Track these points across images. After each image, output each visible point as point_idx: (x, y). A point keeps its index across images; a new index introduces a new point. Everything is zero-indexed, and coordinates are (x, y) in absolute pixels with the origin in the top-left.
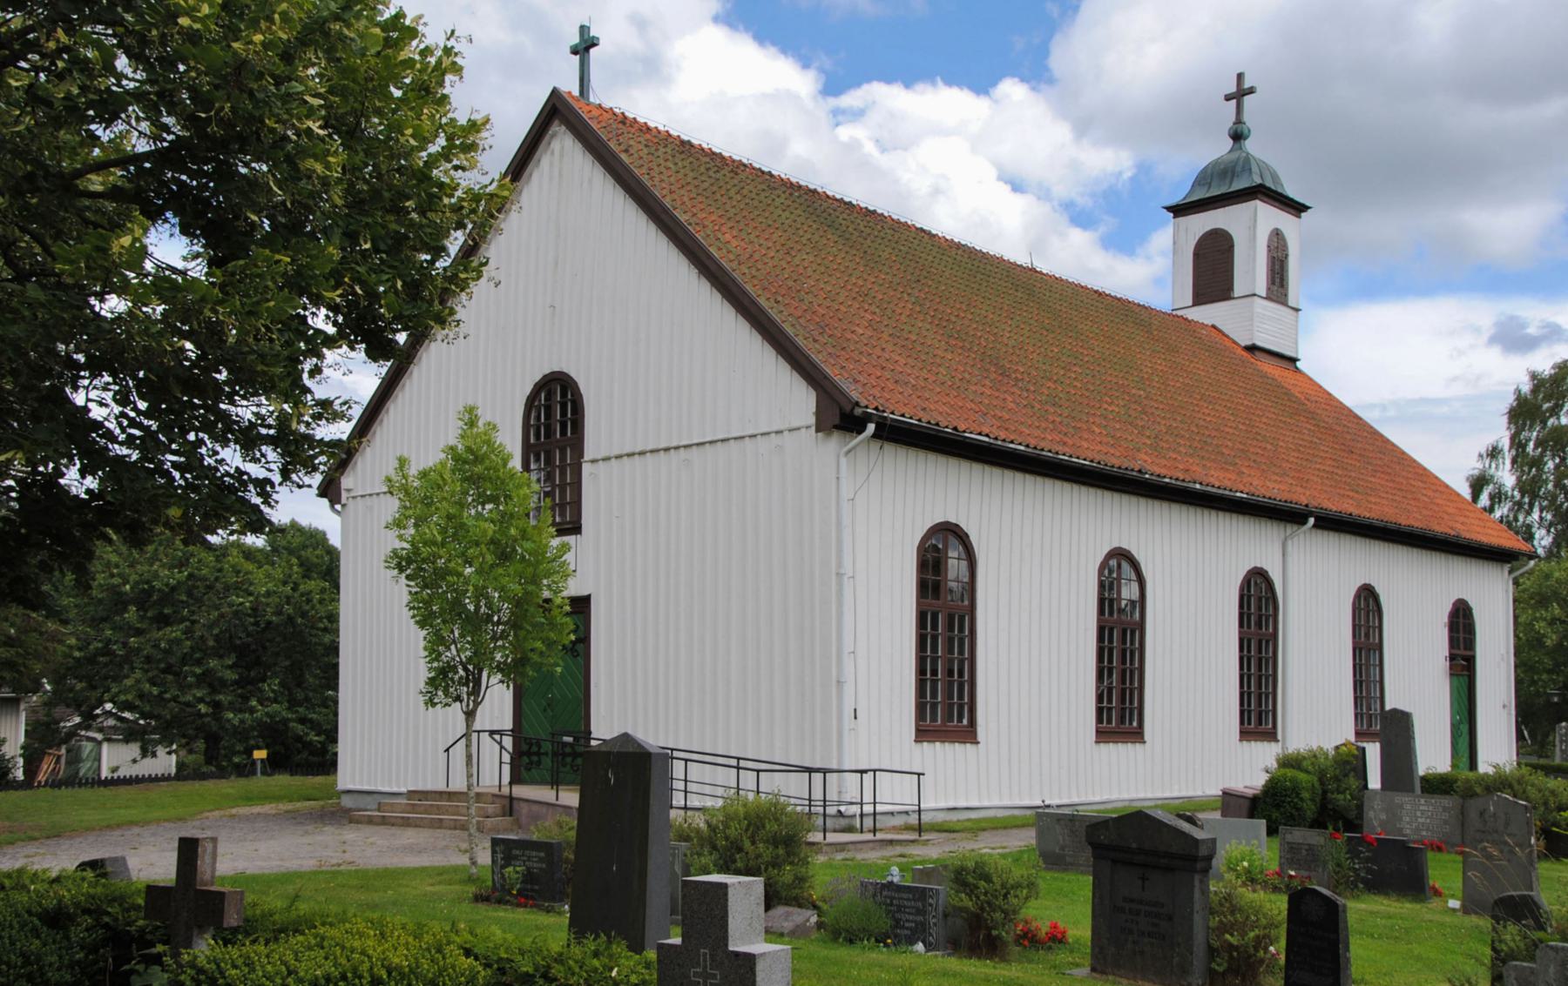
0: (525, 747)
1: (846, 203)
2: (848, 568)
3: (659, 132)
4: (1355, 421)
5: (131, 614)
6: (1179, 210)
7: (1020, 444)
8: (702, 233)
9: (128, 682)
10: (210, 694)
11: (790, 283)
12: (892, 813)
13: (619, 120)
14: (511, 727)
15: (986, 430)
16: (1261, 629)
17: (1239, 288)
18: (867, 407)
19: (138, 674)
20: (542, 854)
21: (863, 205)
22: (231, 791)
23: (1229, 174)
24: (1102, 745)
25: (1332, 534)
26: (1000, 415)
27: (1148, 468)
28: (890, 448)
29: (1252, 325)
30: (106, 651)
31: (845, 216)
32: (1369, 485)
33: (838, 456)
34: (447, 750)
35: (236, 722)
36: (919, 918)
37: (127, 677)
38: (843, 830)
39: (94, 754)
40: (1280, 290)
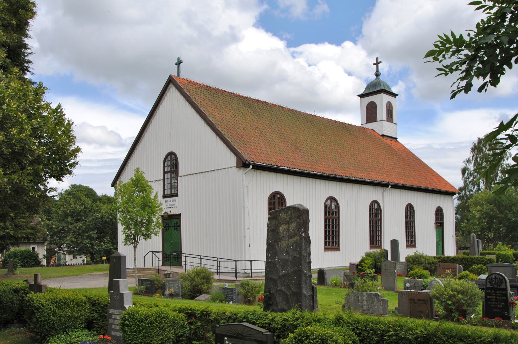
0: (165, 256)
1: (257, 100)
2: (246, 205)
3: (200, 84)
4: (412, 156)
5: (69, 219)
6: (362, 96)
7: (297, 169)
8: (208, 113)
9: (68, 238)
10: (90, 241)
11: (233, 126)
12: (261, 272)
13: (188, 82)
14: (161, 250)
15: (287, 166)
16: (376, 217)
17: (379, 118)
18: (250, 161)
19: (71, 236)
20: (150, 283)
21: (262, 100)
22: (92, 268)
23: (375, 86)
24: (326, 252)
25: (398, 190)
26: (293, 161)
27: (338, 174)
28: (256, 171)
29: (382, 129)
30: (63, 229)
31: (255, 104)
32: (411, 175)
33: (243, 174)
34: (144, 257)
35: (97, 249)
36: (232, 296)
37: (68, 236)
38: (246, 277)
39: (64, 258)
40: (391, 118)
